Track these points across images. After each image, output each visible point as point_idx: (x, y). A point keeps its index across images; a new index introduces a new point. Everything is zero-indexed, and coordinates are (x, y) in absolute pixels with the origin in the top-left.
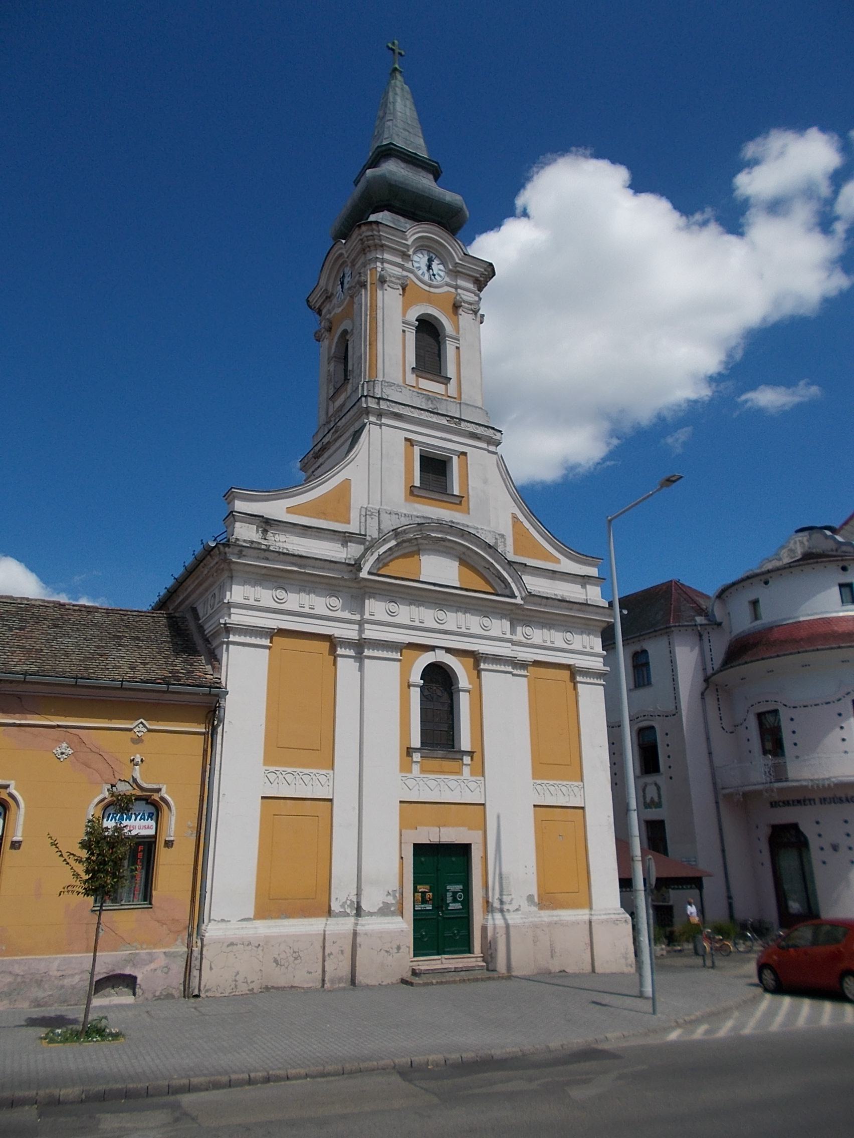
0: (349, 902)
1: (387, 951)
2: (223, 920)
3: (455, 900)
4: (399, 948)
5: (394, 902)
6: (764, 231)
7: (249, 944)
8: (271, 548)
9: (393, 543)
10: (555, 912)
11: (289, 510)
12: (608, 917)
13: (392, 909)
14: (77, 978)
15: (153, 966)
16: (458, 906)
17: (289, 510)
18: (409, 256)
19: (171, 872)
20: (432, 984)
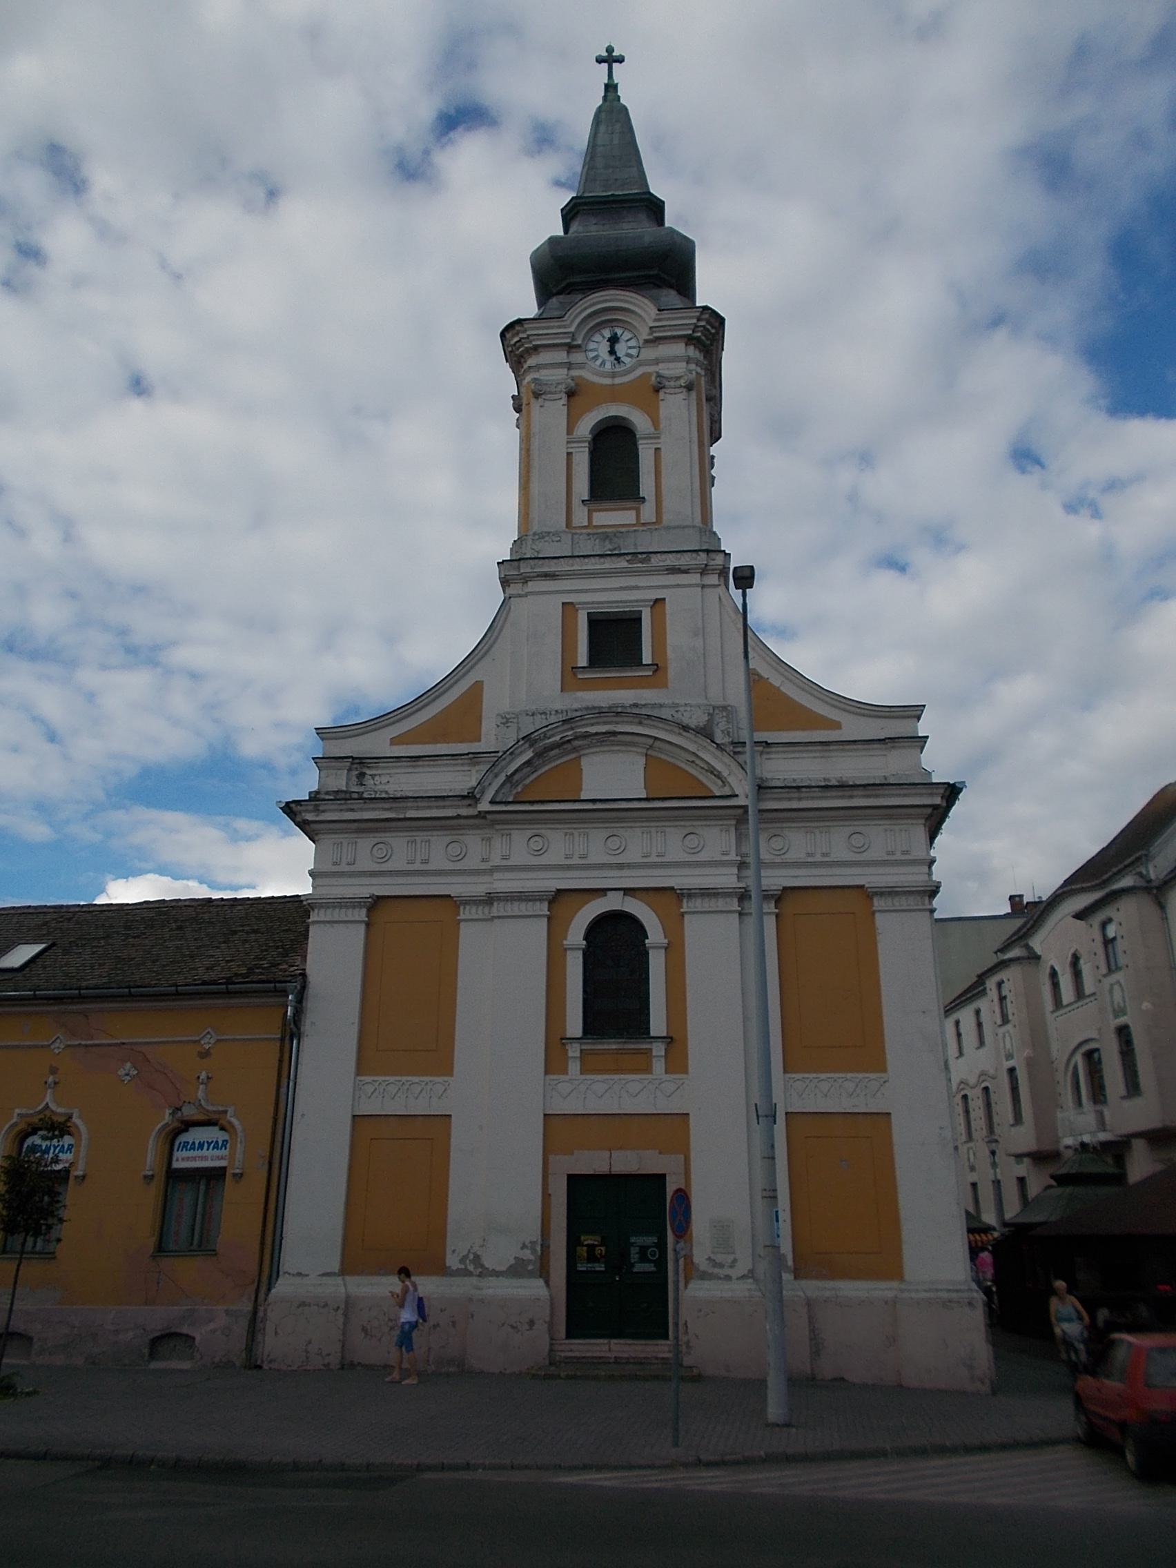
0: (471, 1257)
1: (512, 1327)
2: (299, 1274)
3: (643, 1258)
4: (532, 1323)
5: (532, 1257)
6: (299, 218)
7: (326, 1305)
8: (365, 795)
9: (529, 754)
10: (831, 1284)
11: (394, 741)
12: (954, 1295)
13: (530, 1268)
14: (131, 1334)
15: (212, 1326)
16: (650, 1267)
17: (394, 741)
18: (579, 346)
19: (237, 1213)
20: (559, 1377)
